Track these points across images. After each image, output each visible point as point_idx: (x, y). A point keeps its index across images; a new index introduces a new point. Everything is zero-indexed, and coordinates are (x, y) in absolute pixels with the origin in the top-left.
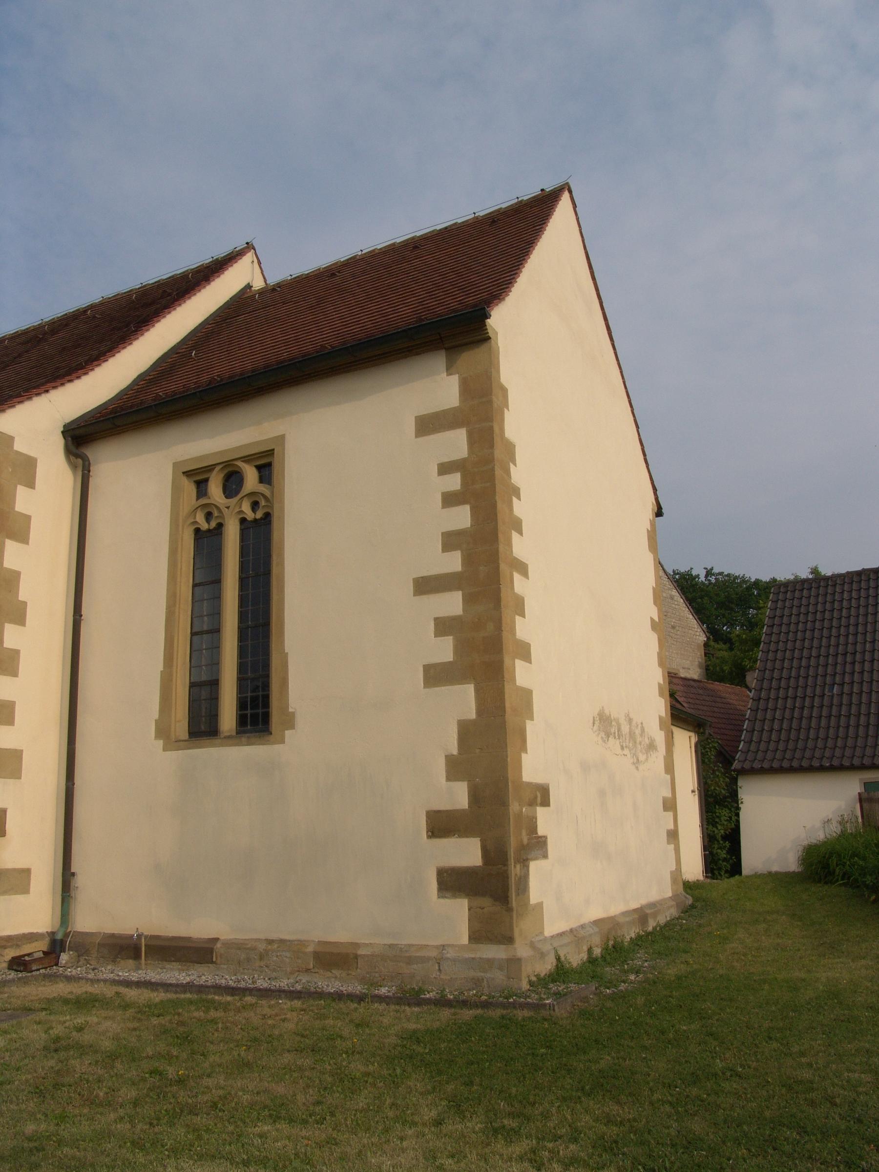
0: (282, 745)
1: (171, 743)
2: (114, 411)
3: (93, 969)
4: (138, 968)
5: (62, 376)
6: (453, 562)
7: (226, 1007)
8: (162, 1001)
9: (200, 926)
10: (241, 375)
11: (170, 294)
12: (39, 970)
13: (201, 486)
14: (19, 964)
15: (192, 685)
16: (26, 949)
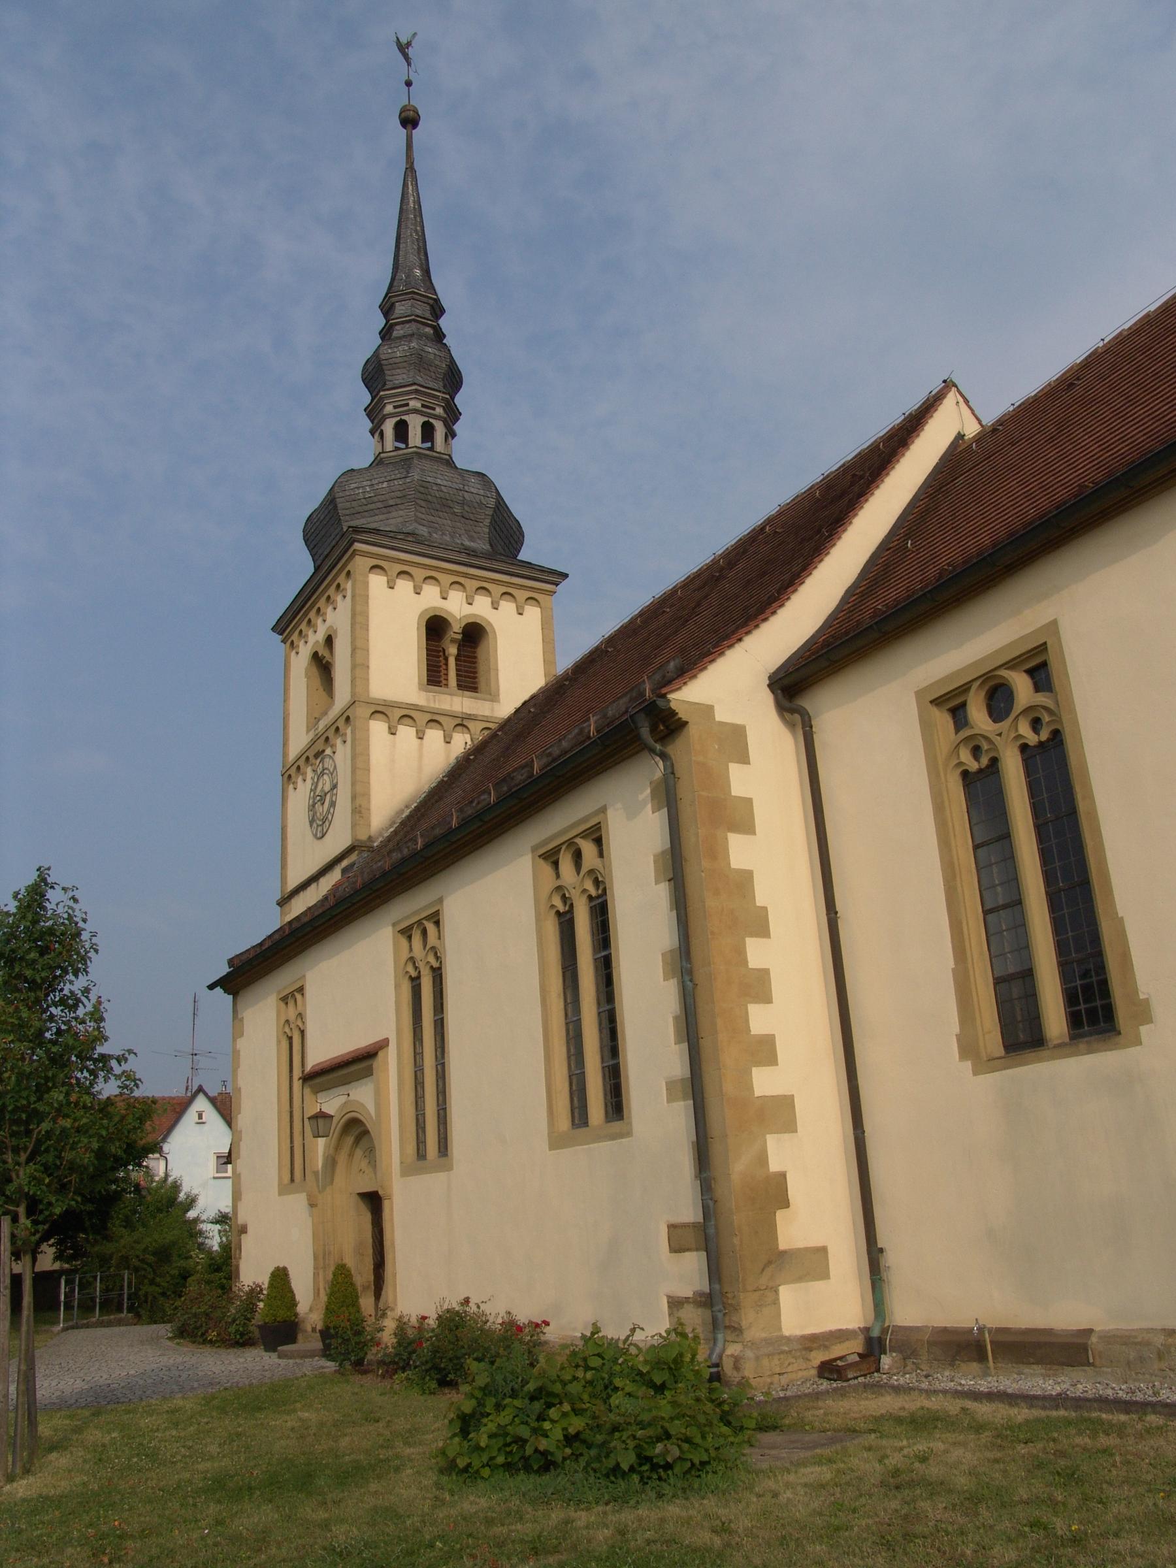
0: (1138, 1048)
1: (983, 1064)
2: (826, 644)
3: (927, 1376)
4: (985, 1374)
5: (755, 616)
7: (1121, 1431)
8: (1027, 1421)
9: (1064, 1313)
10: (978, 555)
11: (861, 477)
12: (856, 1378)
13: (958, 714)
14: (831, 1371)
15: (998, 981)
16: (837, 1351)
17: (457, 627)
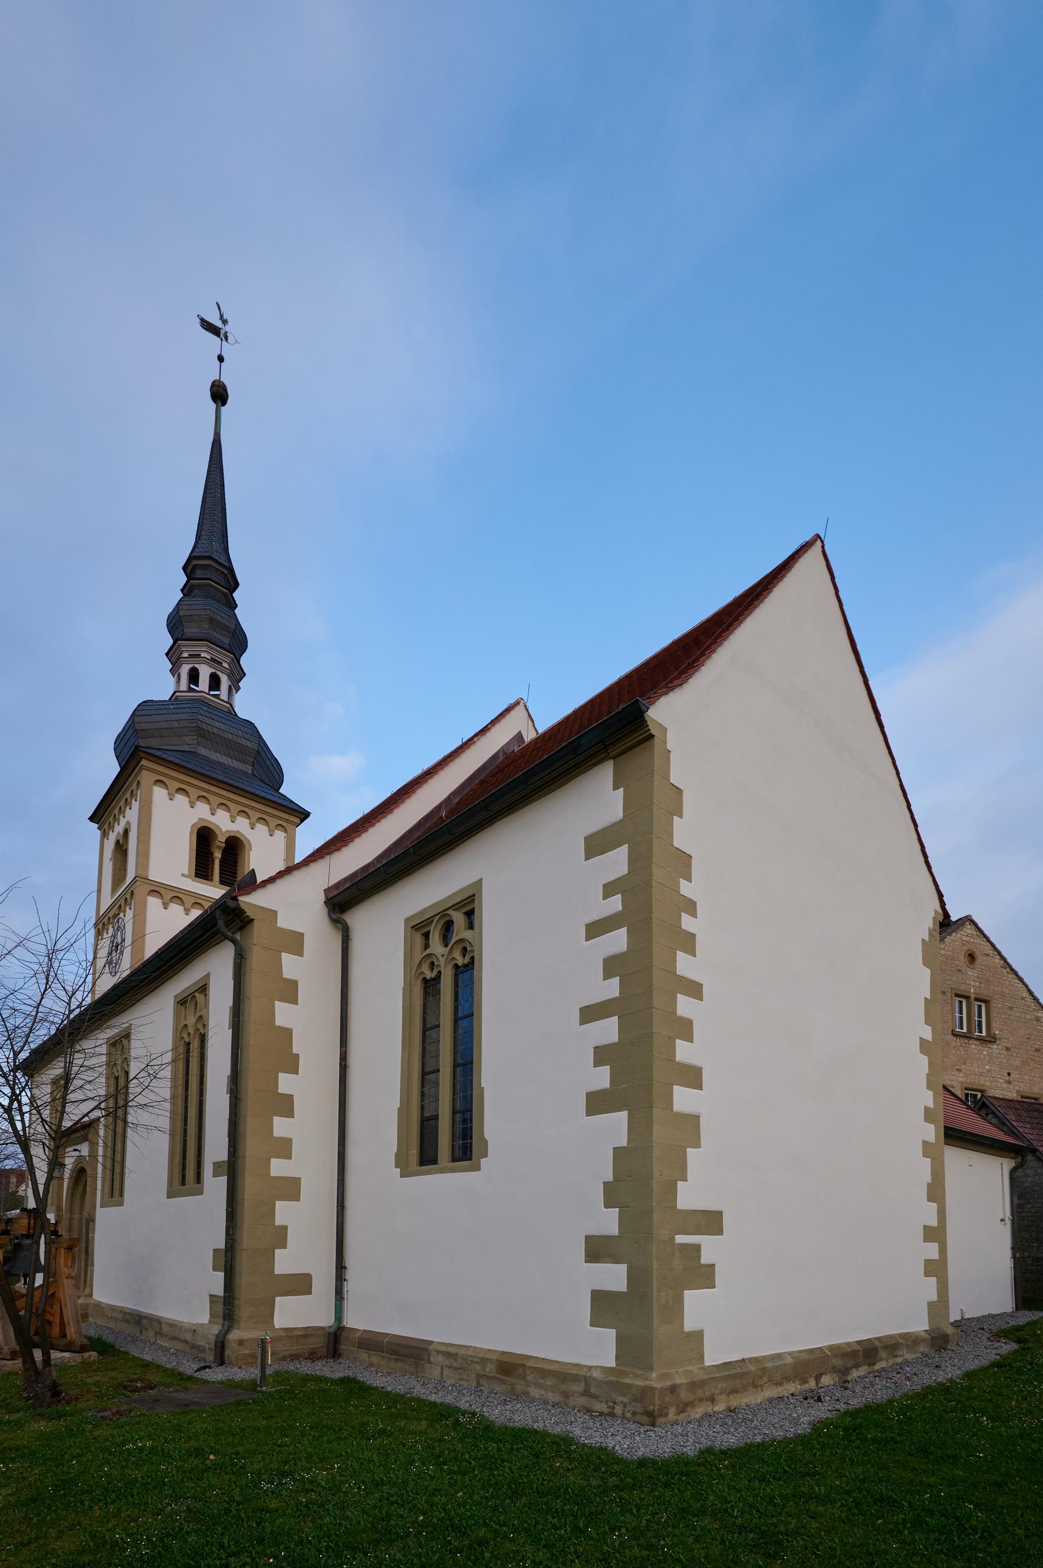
6: (612, 989)
17: (222, 839)
